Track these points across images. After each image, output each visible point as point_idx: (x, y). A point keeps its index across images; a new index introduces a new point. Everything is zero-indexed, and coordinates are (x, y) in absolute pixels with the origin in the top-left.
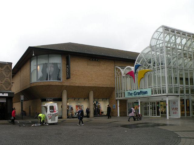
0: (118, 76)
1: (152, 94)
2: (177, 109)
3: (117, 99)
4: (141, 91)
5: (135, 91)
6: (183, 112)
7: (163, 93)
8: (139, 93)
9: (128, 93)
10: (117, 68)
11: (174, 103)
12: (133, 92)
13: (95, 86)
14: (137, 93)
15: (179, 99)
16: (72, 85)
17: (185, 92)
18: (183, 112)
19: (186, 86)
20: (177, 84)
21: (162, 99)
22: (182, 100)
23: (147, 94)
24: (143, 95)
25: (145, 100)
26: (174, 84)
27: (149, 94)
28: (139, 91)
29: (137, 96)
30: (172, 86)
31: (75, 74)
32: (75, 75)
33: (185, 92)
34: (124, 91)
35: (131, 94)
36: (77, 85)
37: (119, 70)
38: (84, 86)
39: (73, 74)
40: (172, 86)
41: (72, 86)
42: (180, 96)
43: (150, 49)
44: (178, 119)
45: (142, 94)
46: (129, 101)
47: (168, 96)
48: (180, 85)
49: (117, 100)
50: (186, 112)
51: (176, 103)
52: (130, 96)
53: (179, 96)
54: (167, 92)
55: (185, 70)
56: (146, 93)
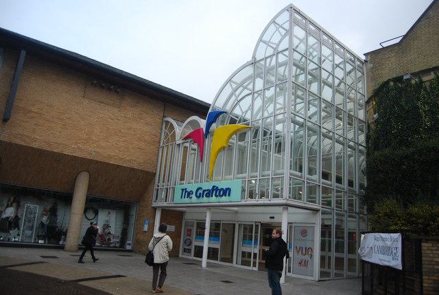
0: (167, 142)
1: (243, 198)
2: (309, 251)
3: (154, 205)
4: (214, 187)
5: (199, 185)
6: (326, 254)
7: (276, 196)
8: (209, 193)
9: (183, 190)
10: (167, 122)
11: (304, 233)
12: (192, 187)
13: (95, 159)
14: (204, 191)
15: (317, 221)
16: (19, 142)
17: (334, 204)
18: (326, 254)
19: (337, 187)
20: (314, 177)
21: (273, 218)
22: (325, 229)
23: (229, 195)
24: (219, 199)
25: (224, 217)
26: (330, 258)
27: (235, 197)
28: (207, 186)
29: (205, 199)
30: (301, 177)
31: (36, 113)
32: (36, 115)
33: (334, 204)
34: (175, 184)
35: (189, 194)
36: (35, 145)
37: (172, 127)
38: (58, 153)
39: (30, 111)
40: (301, 177)
41: (16, 145)
42: (320, 213)
43: (249, 71)
44: (307, 284)
45: (216, 196)
46: (187, 217)
47: (286, 206)
48: (322, 180)
49: (155, 209)
50: (334, 240)
51: (309, 232)
52: (187, 200)
53: (317, 211)
54: (286, 193)
55: (337, 191)
56: (226, 192)
